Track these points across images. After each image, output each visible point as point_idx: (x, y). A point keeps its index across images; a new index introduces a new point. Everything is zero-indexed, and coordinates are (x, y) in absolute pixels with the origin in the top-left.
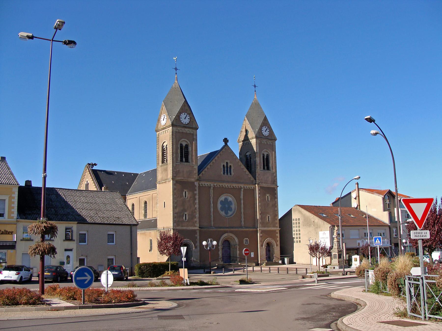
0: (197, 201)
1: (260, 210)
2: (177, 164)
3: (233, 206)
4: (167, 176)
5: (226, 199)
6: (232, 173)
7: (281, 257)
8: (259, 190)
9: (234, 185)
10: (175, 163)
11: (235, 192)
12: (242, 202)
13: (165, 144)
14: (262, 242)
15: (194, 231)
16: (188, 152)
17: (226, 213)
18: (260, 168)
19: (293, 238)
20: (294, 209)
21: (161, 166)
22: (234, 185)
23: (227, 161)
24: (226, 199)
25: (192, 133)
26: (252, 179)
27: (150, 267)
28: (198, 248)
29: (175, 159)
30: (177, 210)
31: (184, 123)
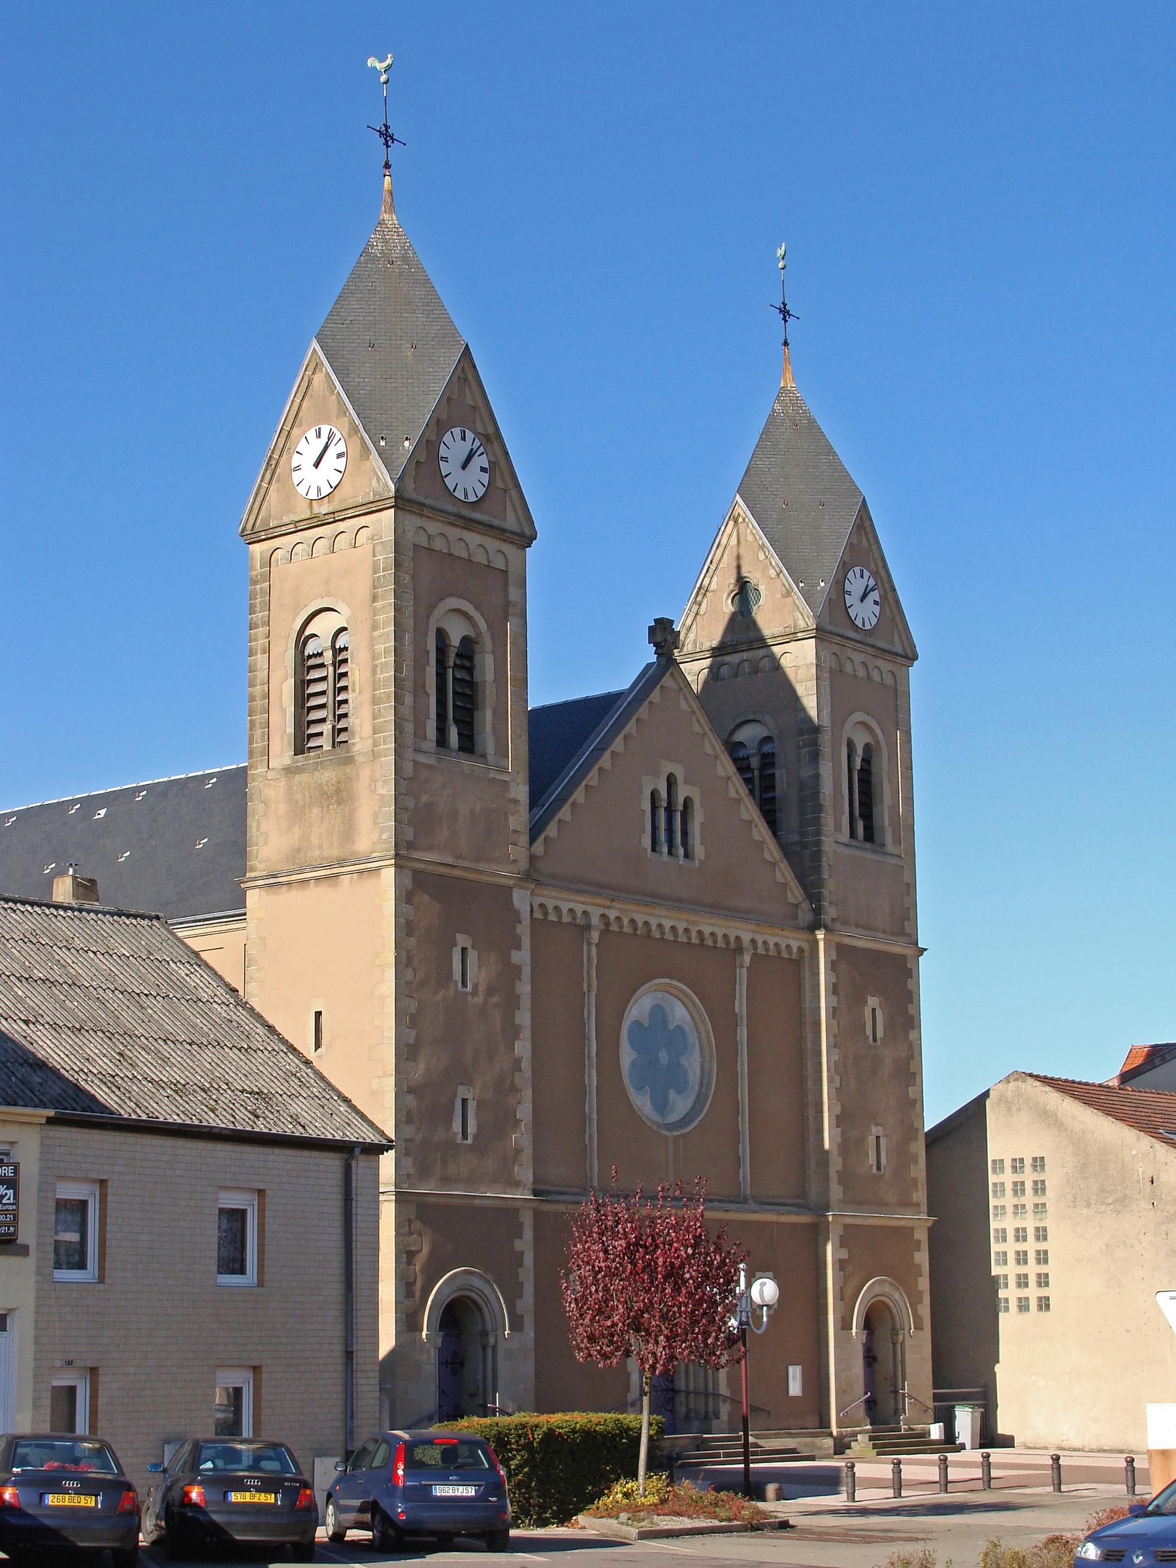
0: (524, 1018)
1: (838, 1093)
2: (422, 759)
3: (693, 1064)
4: (348, 832)
5: (659, 1014)
6: (699, 850)
7: (936, 1398)
8: (833, 966)
9: (710, 925)
10: (409, 754)
11: (703, 967)
12: (743, 1033)
13: (323, 627)
14: (846, 1300)
15: (508, 1214)
16: (471, 684)
17: (662, 1105)
18: (838, 828)
19: (993, 1284)
20: (1001, 1098)
21: (288, 771)
22: (710, 925)
23: (668, 767)
24: (659, 1014)
25: (499, 563)
26: (795, 893)
27: (529, 1447)
28: (529, 1332)
29: (409, 727)
30: (418, 1073)
31: (459, 494)
